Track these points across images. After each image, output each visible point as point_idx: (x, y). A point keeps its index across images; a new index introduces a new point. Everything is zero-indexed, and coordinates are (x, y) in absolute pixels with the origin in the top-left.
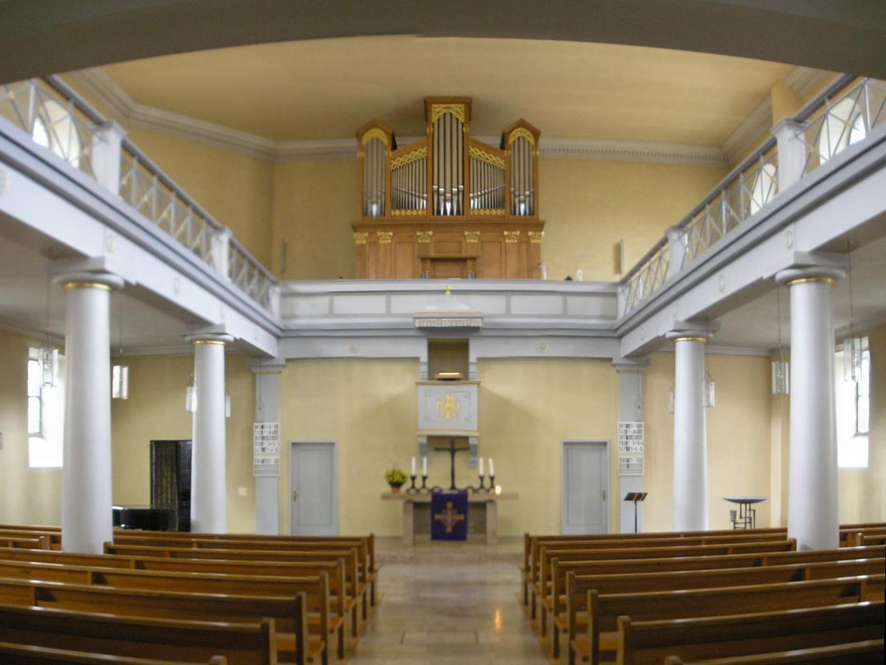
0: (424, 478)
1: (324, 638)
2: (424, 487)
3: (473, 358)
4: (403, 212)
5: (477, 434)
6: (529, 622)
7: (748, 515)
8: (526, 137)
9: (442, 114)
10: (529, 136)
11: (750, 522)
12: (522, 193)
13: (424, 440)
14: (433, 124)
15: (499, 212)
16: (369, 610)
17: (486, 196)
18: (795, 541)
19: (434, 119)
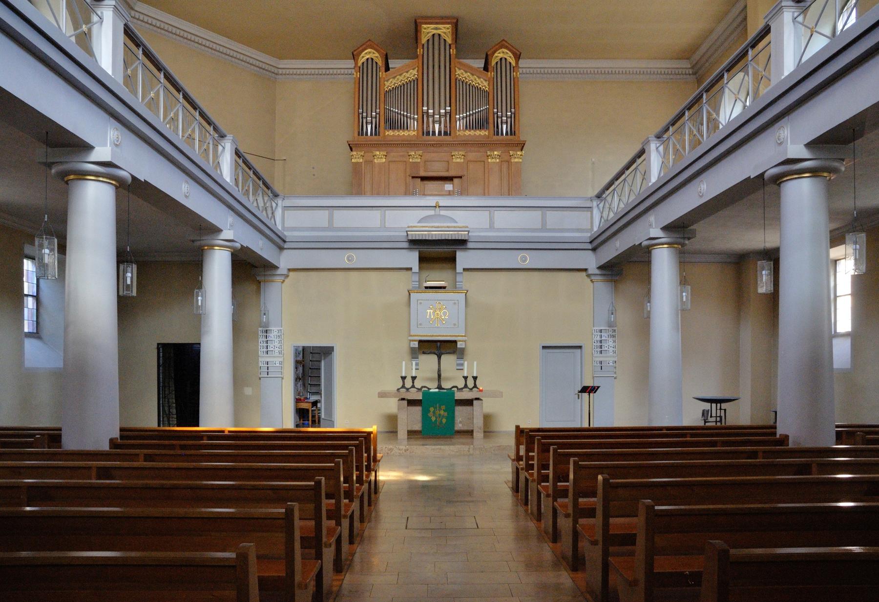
0: (414, 378)
1: (339, 523)
2: (413, 386)
3: (459, 268)
4: (396, 133)
5: (464, 338)
6: (521, 509)
7: (718, 415)
8: (508, 58)
9: (431, 34)
10: (510, 57)
11: (721, 421)
12: (504, 114)
13: (416, 345)
14: (423, 45)
15: (483, 133)
16: (373, 496)
17: (477, 114)
18: (787, 437)
19: (424, 40)
